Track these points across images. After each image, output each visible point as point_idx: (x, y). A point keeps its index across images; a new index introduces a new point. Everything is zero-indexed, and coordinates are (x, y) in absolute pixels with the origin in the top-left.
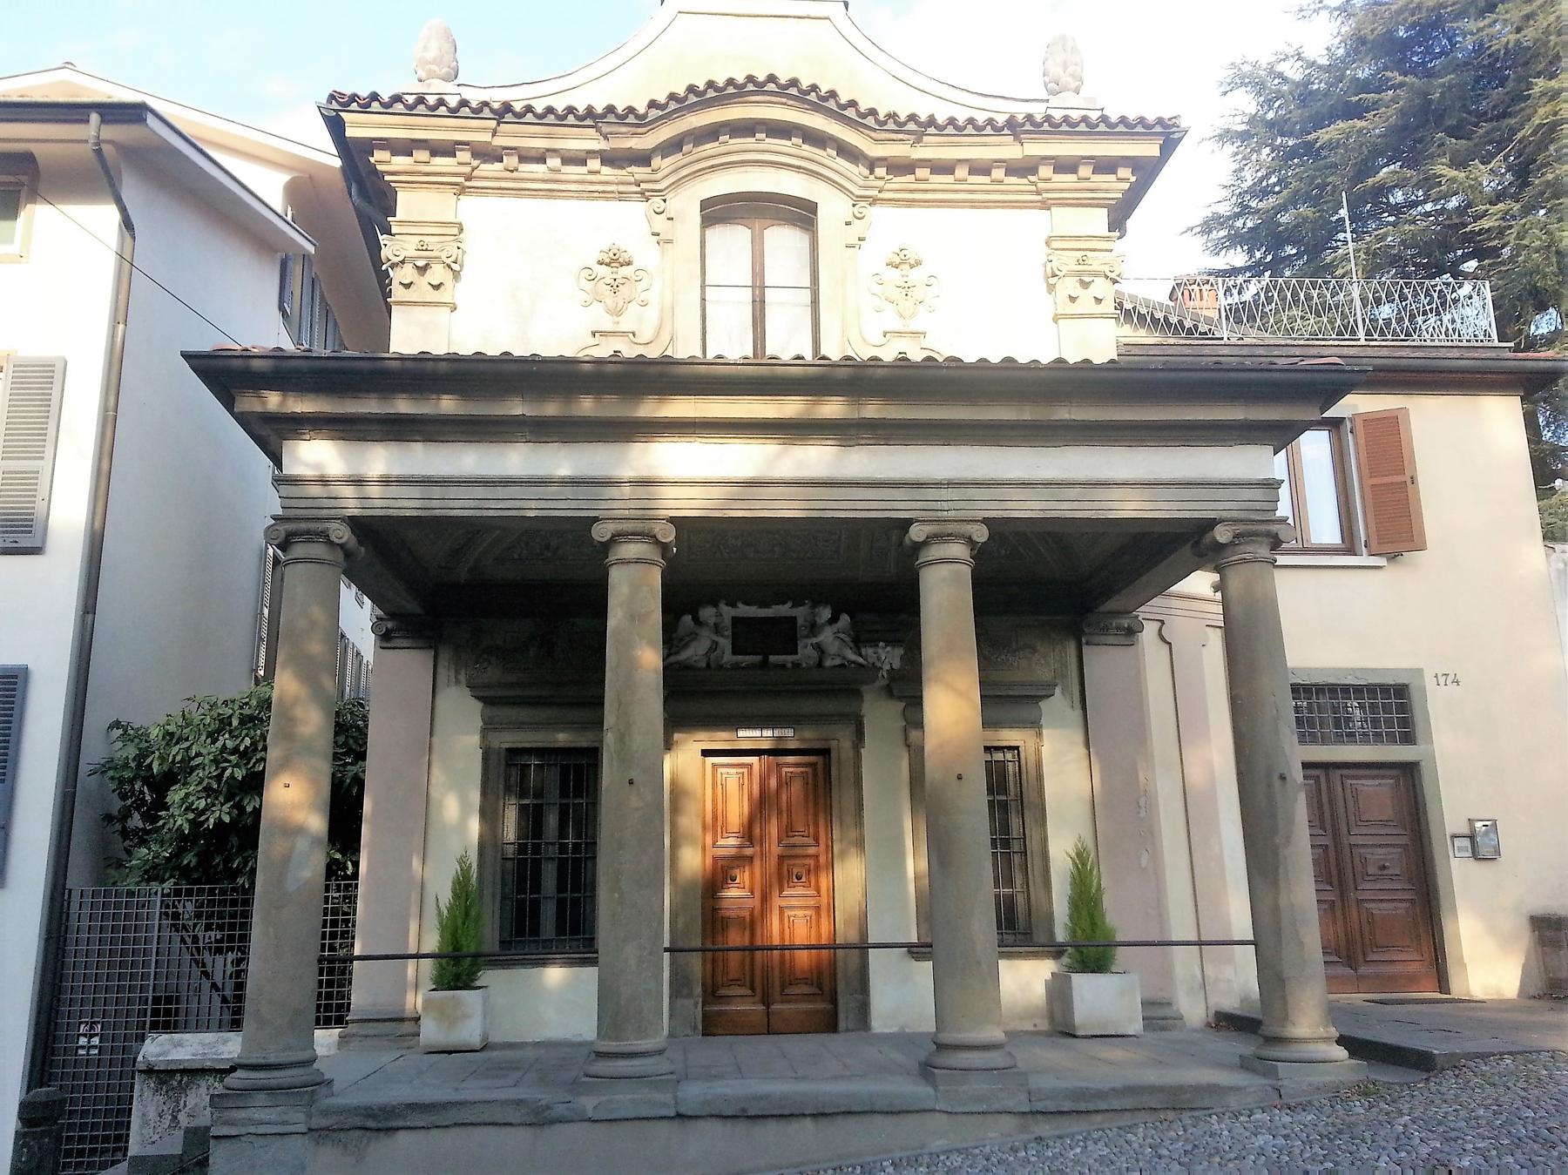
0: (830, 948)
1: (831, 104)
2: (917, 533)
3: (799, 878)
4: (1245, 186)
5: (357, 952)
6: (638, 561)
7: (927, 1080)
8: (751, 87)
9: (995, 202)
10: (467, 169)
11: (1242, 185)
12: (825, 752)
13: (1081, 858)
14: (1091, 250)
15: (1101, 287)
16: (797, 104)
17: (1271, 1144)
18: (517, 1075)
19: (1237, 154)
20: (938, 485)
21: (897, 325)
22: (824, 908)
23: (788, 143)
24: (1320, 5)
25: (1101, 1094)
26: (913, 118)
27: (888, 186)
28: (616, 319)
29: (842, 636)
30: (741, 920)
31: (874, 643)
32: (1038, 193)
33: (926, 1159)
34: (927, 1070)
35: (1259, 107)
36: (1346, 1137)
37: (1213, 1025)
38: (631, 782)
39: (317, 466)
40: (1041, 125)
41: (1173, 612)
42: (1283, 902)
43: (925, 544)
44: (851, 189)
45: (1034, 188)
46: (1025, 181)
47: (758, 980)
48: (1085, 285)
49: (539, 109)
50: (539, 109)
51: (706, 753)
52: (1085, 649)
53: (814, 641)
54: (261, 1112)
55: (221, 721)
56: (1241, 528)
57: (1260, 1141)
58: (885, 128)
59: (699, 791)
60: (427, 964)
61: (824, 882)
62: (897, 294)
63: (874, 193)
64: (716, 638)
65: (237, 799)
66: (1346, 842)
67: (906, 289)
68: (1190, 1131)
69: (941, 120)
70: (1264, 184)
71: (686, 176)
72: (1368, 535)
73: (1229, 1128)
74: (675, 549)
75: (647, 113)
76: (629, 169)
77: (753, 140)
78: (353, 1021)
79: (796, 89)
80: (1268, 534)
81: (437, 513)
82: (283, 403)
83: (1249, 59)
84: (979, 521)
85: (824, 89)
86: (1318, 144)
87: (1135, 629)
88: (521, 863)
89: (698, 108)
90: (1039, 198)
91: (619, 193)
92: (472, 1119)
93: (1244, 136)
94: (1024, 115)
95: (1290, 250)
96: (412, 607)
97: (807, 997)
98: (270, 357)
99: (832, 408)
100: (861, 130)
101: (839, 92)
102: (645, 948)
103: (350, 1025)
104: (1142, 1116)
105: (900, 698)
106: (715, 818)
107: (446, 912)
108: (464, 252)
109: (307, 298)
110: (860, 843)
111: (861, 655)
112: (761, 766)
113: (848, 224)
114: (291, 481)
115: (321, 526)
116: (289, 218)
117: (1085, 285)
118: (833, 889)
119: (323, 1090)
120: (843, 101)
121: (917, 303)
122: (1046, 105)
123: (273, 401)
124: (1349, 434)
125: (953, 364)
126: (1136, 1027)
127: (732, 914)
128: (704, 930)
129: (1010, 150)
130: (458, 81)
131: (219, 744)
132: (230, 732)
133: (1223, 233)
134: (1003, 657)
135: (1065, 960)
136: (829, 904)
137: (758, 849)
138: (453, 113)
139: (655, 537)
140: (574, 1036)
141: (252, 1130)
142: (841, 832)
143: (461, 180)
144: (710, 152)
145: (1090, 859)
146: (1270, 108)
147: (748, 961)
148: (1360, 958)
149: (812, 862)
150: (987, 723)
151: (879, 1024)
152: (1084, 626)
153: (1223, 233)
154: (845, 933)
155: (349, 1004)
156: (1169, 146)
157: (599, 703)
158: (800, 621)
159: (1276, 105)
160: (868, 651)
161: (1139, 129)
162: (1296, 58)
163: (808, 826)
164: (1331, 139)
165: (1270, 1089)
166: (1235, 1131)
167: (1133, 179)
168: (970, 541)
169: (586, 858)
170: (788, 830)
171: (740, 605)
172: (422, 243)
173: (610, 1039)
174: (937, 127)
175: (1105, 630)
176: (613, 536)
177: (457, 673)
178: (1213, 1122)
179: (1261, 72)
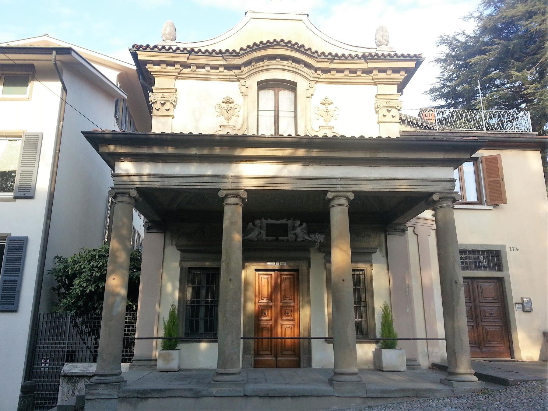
0: (298, 339)
1: (302, 49)
2: (330, 196)
4: (445, 77)
5: (136, 336)
6: (234, 204)
7: (331, 385)
8: (275, 43)
10: (179, 71)
12: (297, 271)
13: (385, 309)
14: (391, 99)
15: (394, 112)
16: (291, 49)
20: (337, 179)
21: (324, 124)
22: (296, 325)
23: (287, 62)
24: (471, 16)
26: (330, 54)
27: (321, 77)
28: (228, 121)
30: (267, 329)
31: (314, 233)
32: (373, 80)
34: (331, 382)
35: (450, 51)
37: (431, 368)
38: (230, 280)
39: (126, 170)
40: (374, 56)
43: (332, 199)
45: (371, 78)
46: (369, 76)
48: (389, 111)
49: (203, 50)
50: (203, 50)
51: (256, 270)
52: (387, 236)
53: (294, 232)
54: (102, 391)
56: (442, 195)
58: (321, 57)
59: (254, 283)
61: (296, 316)
62: (324, 114)
64: (261, 231)
69: (340, 54)
70: (451, 77)
72: (486, 198)
76: (233, 71)
77: (275, 61)
78: (135, 360)
80: (452, 198)
81: (166, 187)
82: (115, 149)
83: (446, 34)
85: (300, 44)
86: (470, 64)
88: (193, 307)
90: (373, 81)
91: (230, 79)
93: (444, 61)
96: (157, 218)
97: (290, 355)
99: (301, 153)
103: (133, 362)
104: (406, 399)
105: (323, 252)
107: (167, 323)
108: (177, 99)
110: (309, 302)
111: (310, 237)
113: (307, 90)
115: (127, 191)
116: (119, 87)
118: (300, 318)
119: (123, 384)
122: (376, 50)
123: (112, 148)
124: (480, 163)
126: (404, 368)
127: (265, 326)
129: (363, 65)
131: (91, 264)
133: (437, 94)
135: (380, 344)
136: (298, 323)
137: (274, 303)
138: (174, 51)
139: (240, 196)
143: (177, 74)
144: (261, 65)
145: (389, 309)
146: (454, 51)
149: (292, 308)
150: (353, 262)
153: (437, 94)
154: (304, 334)
155: (133, 354)
156: (418, 64)
157: (220, 252)
158: (289, 225)
160: (313, 236)
162: (463, 34)
164: (475, 62)
167: (406, 75)
168: (348, 199)
170: (284, 297)
172: (163, 95)
174: (339, 57)
175: (395, 230)
177: (172, 241)
178: (430, 402)
179: (451, 39)
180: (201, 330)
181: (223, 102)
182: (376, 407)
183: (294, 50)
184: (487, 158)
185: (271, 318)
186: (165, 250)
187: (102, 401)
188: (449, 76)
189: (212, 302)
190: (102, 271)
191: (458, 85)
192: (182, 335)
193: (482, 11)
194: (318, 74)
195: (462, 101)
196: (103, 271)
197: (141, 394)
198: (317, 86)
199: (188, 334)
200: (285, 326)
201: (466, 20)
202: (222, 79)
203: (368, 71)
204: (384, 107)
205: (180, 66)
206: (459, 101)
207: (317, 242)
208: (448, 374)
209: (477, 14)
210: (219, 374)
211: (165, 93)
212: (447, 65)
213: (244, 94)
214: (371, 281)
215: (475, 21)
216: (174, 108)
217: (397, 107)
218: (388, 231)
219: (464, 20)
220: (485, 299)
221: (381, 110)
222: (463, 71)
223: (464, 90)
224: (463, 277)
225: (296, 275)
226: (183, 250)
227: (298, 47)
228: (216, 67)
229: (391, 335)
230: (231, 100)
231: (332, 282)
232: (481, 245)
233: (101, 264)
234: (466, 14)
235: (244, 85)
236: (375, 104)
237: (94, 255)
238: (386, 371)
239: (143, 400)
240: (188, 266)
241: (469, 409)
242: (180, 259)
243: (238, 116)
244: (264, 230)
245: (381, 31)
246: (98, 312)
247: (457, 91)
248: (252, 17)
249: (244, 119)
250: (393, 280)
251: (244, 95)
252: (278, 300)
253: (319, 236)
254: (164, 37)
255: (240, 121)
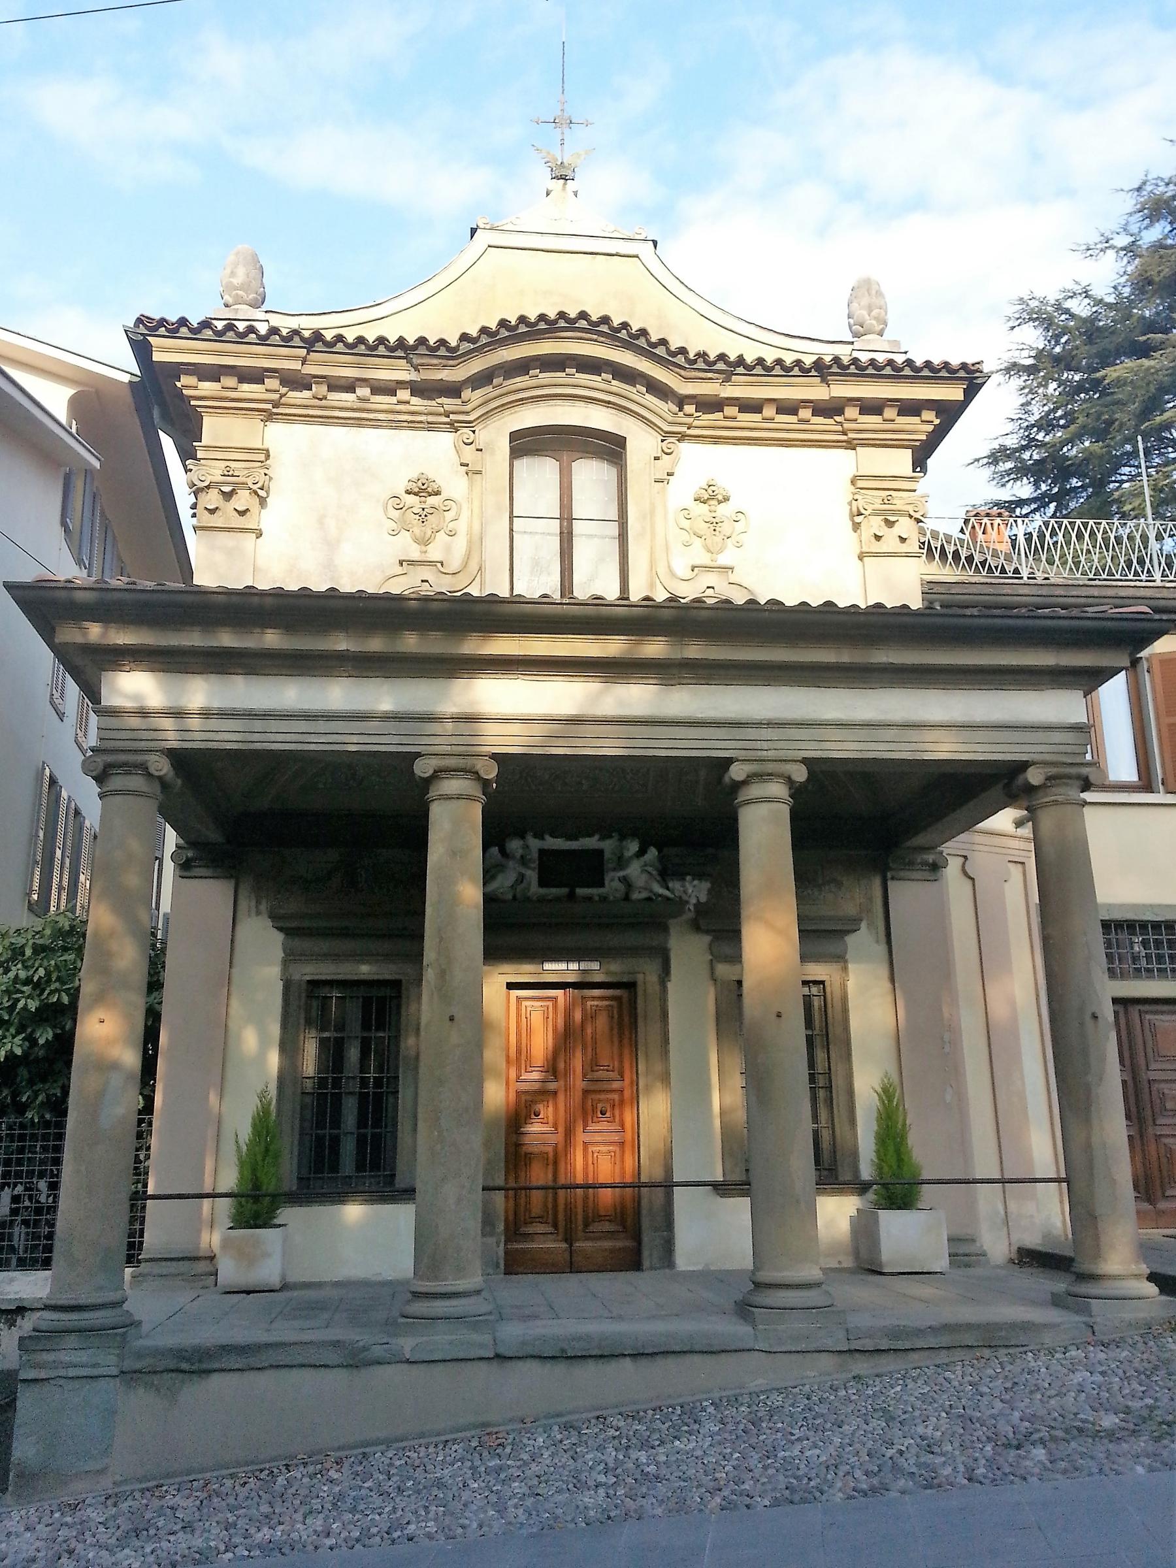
0: (634, 1187)
1: (642, 342)
2: (737, 772)
3: (603, 1113)
4: (1032, 419)
5: (151, 1190)
6: (459, 797)
7: (745, 1320)
8: (562, 323)
9: (802, 441)
10: (276, 396)
11: (1029, 419)
12: (631, 986)
13: (887, 1093)
14: (895, 490)
15: (905, 526)
16: (608, 341)
17: (1090, 1381)
18: (326, 1316)
19: (1024, 388)
20: (758, 724)
21: (705, 559)
22: (631, 1143)
23: (598, 378)
24: (1107, 245)
25: (919, 1332)
26: (722, 357)
27: (696, 423)
28: (424, 548)
29: (650, 869)
30: (544, 1156)
31: (681, 877)
32: (844, 433)
33: (746, 1399)
34: (744, 1309)
35: (1046, 342)
36: (1162, 1373)
37: (1016, 1262)
38: (452, 1019)
39: (136, 697)
40: (848, 367)
41: (977, 847)
42: (1095, 1140)
43: (745, 783)
44: (660, 425)
45: (839, 428)
46: (831, 421)
47: (561, 1216)
48: (890, 524)
49: (350, 339)
50: (350, 339)
51: (511, 986)
52: (889, 883)
53: (621, 874)
54: (71, 1354)
55: (13, 950)
56: (1053, 771)
57: (1078, 1377)
58: (695, 366)
59: (504, 1024)
60: (224, 1204)
61: (628, 1118)
62: (703, 528)
63: (684, 429)
64: (523, 871)
65: (29, 1030)
66: (1144, 1077)
67: (715, 524)
68: (1007, 1369)
69: (749, 359)
70: (1052, 416)
71: (496, 408)
72: (1164, 773)
73: (1045, 1365)
74: (494, 785)
75: (458, 346)
76: (439, 401)
77: (563, 374)
78: (147, 1260)
79: (607, 326)
80: (1079, 777)
81: (258, 746)
82: (104, 635)
83: (1037, 294)
84: (798, 761)
85: (635, 327)
86: (1107, 381)
87: (940, 864)
88: (321, 1097)
89: (509, 342)
90: (844, 438)
91: (428, 423)
92: (288, 1361)
93: (1031, 370)
94: (832, 357)
95: (1075, 482)
96: (214, 835)
97: (611, 1235)
98: (92, 589)
99: (655, 648)
100: (671, 367)
101: (650, 331)
102: (464, 1187)
103: (143, 1265)
104: (959, 1354)
105: (707, 932)
106: (519, 1051)
107: (245, 1148)
108: (271, 479)
109: (87, 514)
110: (665, 1078)
111: (668, 888)
112: (565, 1000)
113: (656, 458)
114: (111, 712)
115: (140, 758)
116: (74, 430)
117: (890, 524)
118: (638, 1124)
119: (132, 1331)
120: (654, 339)
121: (725, 538)
122: (850, 347)
123: (95, 632)
124: (1146, 673)
125: (775, 607)
126: (941, 1263)
127: (535, 1150)
128: (507, 1167)
129: (818, 392)
130: (265, 307)
131: (11, 975)
132: (23, 962)
133: (1009, 465)
134: (810, 891)
135: (871, 1196)
136: (633, 1139)
137: (562, 1083)
138: (263, 340)
139: (477, 773)
140: (373, 1275)
141: (62, 1373)
142: (647, 1061)
143: (269, 406)
144: (520, 386)
145: (897, 1095)
146: (1057, 343)
147: (550, 1199)
148: (1159, 1193)
149: (616, 1097)
150: (804, 958)
151: (683, 1262)
152: (890, 861)
153: (1009, 465)
154: (651, 1171)
155: (141, 1243)
156: (972, 390)
157: (418, 936)
158: (607, 855)
159: (1063, 340)
160: (675, 885)
161: (944, 374)
162: (1084, 295)
163: (612, 1058)
164: (1119, 377)
165: (1083, 1326)
166: (1053, 1368)
167: (937, 421)
168: (789, 781)
169: (387, 1093)
170: (593, 1064)
171: (547, 837)
172: (228, 469)
173: (428, 1280)
174: (747, 367)
175: (911, 864)
176: (435, 772)
177: (258, 902)
178: (1029, 1359)
179: (1049, 309)
180: (348, 1163)
181: (408, 492)
182: (878, 1380)
183: (617, 344)
184: (1166, 657)
185: (555, 1126)
186: (239, 928)
187: (70, 1385)
188: (1043, 414)
189: (378, 1082)
190: (47, 992)
191: (1070, 441)
192: (290, 1183)
193: (1136, 231)
194: (688, 413)
195: (1079, 487)
196: (48, 994)
197: (188, 1360)
198: (685, 448)
199: (309, 1179)
200: (596, 1149)
201: (1091, 255)
202: (405, 424)
203: (830, 409)
204: (876, 513)
205: (278, 382)
206: (1073, 486)
207: (687, 902)
208: (1074, 1278)
209: (1123, 241)
210: (417, 1295)
211: (234, 460)
212: (1040, 385)
213: (470, 468)
214: (845, 1010)
215: (1119, 259)
216: (262, 508)
217: (912, 513)
218: (891, 869)
219: (1088, 254)
220: (1161, 1059)
221: (869, 522)
222: (1085, 401)
223: (1088, 457)
224: (1112, 999)
225: (625, 1000)
226: (280, 921)
227: (630, 335)
228: (389, 389)
229: (905, 1168)
230: (435, 487)
231: (746, 1021)
232: (1151, 905)
233: (41, 972)
234: (1094, 238)
235: (472, 443)
236: (850, 504)
237: (19, 945)
238: (892, 1274)
239: (195, 1377)
240: (308, 978)
241: (1139, 1375)
242: (283, 955)
243: (452, 534)
244: (533, 869)
245: (866, 293)
246: (32, 1118)
247: (1067, 458)
248: (491, 244)
249: (470, 542)
250: (907, 1007)
251: (471, 472)
252: (574, 1071)
253: (694, 886)
254: (230, 295)
255: (460, 545)
